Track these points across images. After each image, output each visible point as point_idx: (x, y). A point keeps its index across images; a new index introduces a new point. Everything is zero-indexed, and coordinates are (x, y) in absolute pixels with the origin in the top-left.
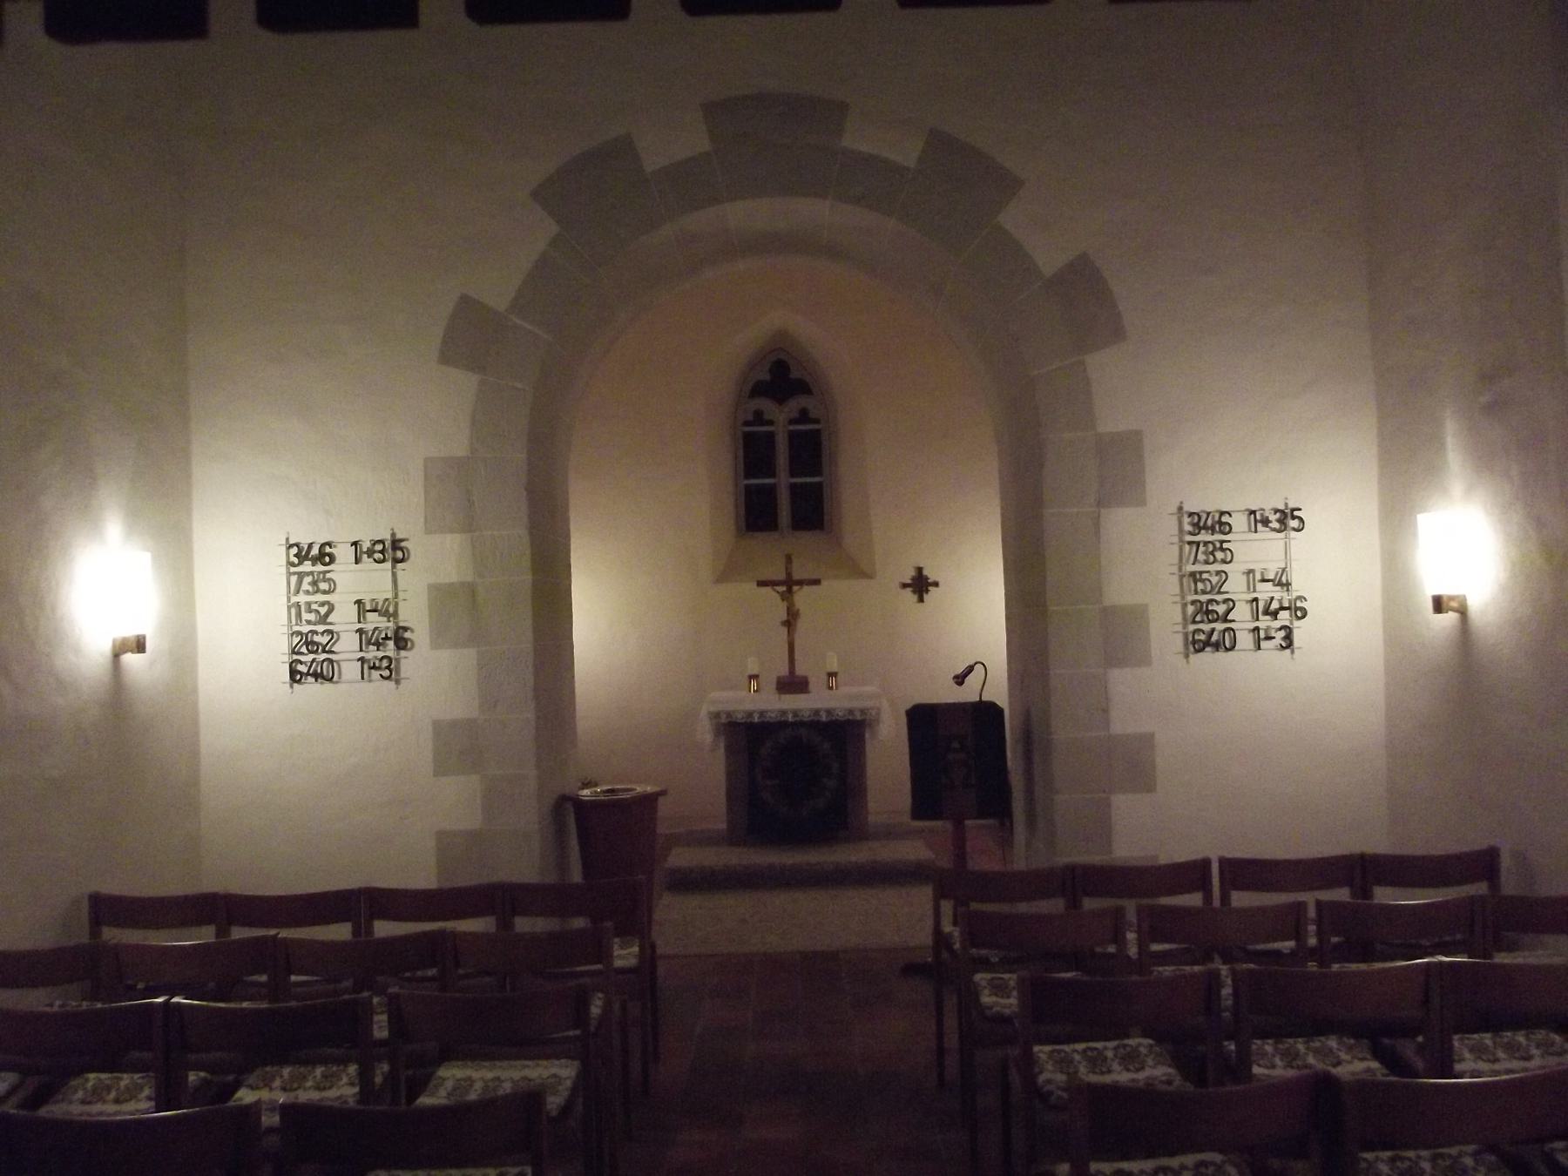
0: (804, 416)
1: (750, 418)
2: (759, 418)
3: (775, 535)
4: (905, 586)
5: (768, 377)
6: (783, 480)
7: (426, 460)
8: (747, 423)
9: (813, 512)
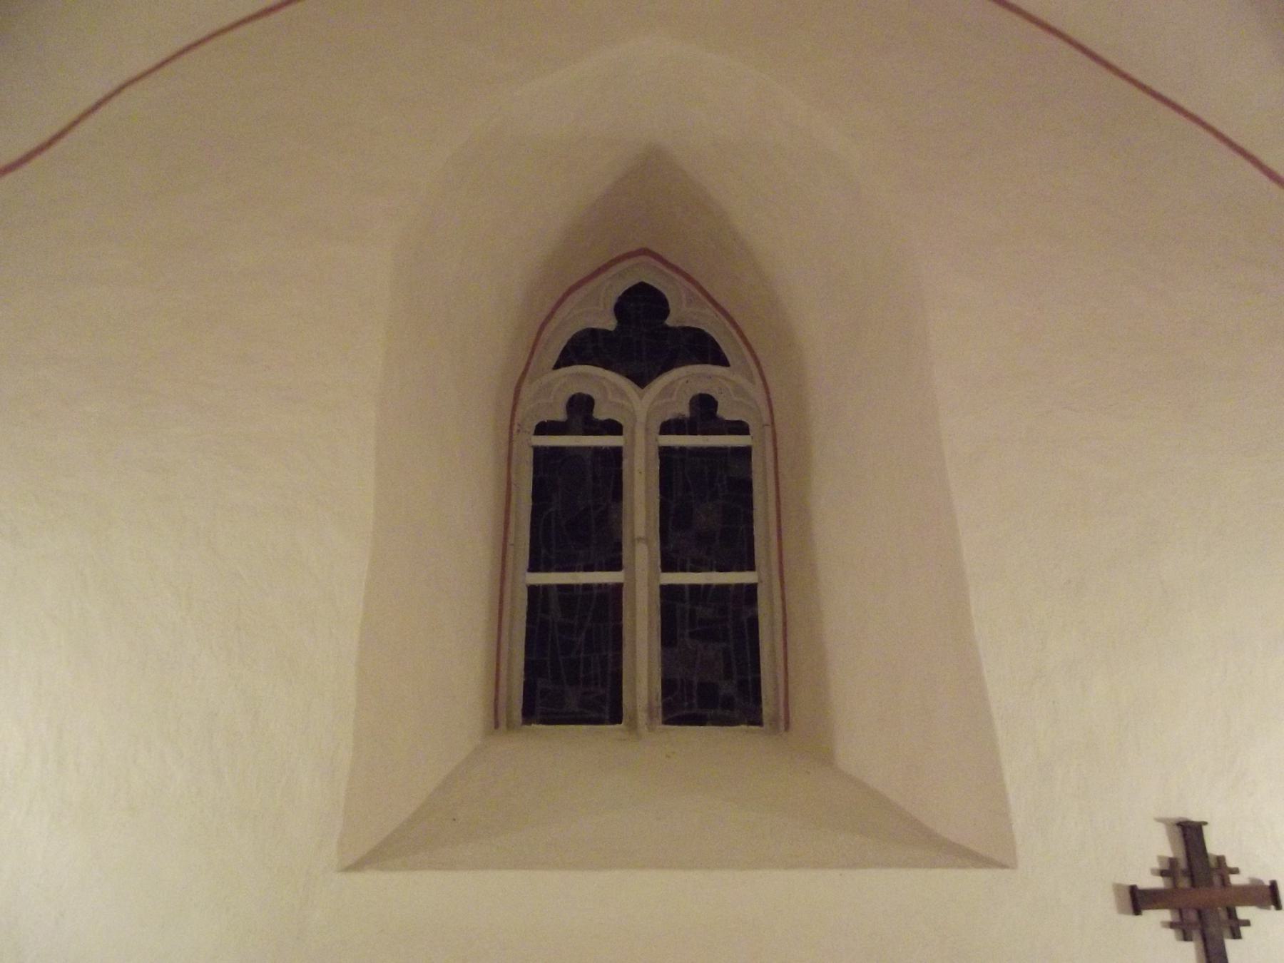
0: (704, 413)
1: (560, 415)
2: (581, 412)
3: (766, 611)
4: (1138, 900)
5: (608, 323)
6: (641, 577)
7: (666, 722)
8: (544, 428)
9: (724, 673)
